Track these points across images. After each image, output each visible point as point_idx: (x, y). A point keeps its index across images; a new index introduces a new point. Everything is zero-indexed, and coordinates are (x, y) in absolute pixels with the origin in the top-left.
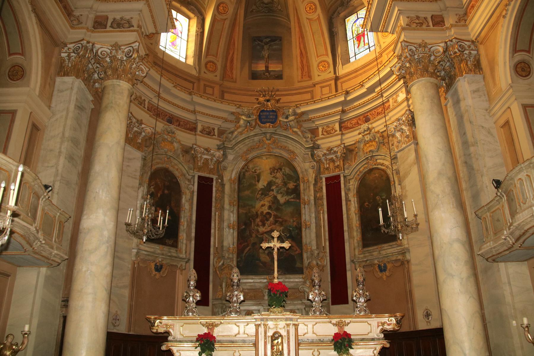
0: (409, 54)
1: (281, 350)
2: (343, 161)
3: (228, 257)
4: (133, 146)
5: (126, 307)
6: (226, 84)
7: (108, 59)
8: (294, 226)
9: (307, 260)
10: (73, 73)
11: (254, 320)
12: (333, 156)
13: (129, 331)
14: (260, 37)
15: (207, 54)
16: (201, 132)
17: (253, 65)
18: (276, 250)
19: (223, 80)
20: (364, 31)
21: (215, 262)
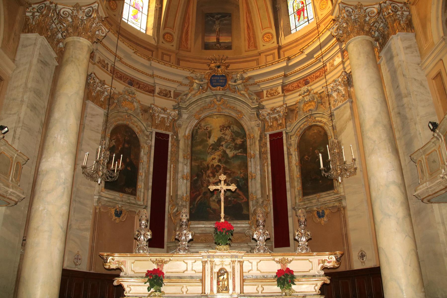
0: (347, 15)
1: (226, 285)
2: (285, 119)
3: (181, 205)
4: (96, 104)
5: (87, 247)
6: (183, 53)
7: (70, 19)
8: (241, 177)
9: (253, 208)
10: (36, 30)
11: (201, 258)
12: (276, 115)
13: (90, 269)
14: (212, 13)
15: (165, 27)
16: (158, 94)
17: (206, 38)
18: (223, 191)
19: (178, 50)
20: (304, 6)
21: (170, 209)
